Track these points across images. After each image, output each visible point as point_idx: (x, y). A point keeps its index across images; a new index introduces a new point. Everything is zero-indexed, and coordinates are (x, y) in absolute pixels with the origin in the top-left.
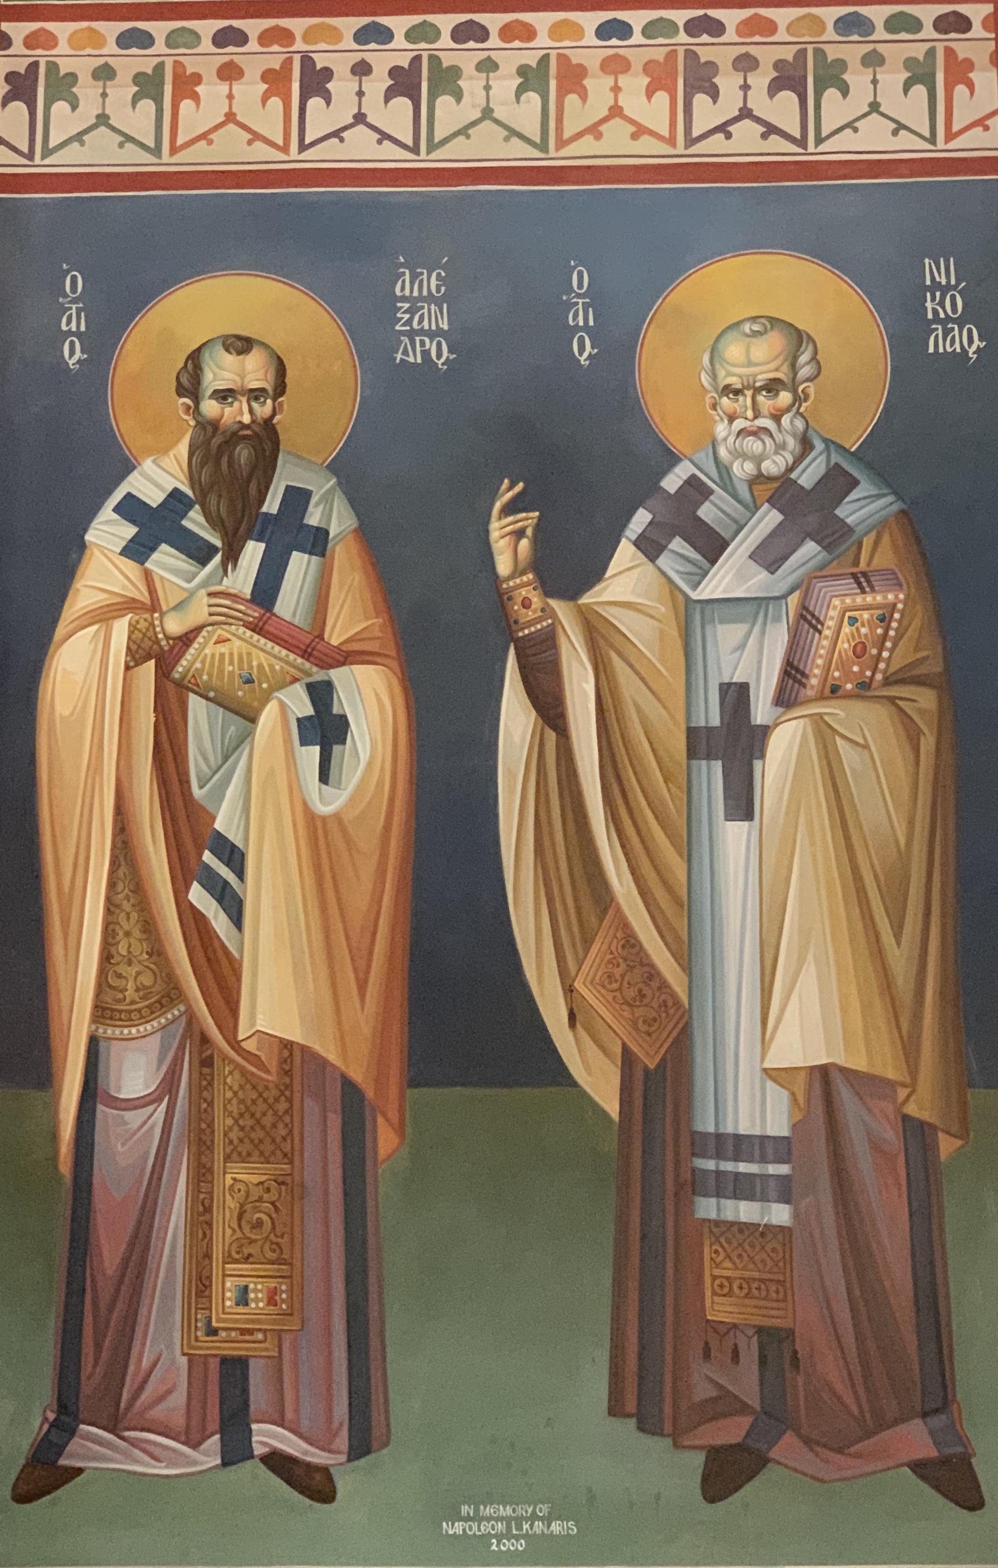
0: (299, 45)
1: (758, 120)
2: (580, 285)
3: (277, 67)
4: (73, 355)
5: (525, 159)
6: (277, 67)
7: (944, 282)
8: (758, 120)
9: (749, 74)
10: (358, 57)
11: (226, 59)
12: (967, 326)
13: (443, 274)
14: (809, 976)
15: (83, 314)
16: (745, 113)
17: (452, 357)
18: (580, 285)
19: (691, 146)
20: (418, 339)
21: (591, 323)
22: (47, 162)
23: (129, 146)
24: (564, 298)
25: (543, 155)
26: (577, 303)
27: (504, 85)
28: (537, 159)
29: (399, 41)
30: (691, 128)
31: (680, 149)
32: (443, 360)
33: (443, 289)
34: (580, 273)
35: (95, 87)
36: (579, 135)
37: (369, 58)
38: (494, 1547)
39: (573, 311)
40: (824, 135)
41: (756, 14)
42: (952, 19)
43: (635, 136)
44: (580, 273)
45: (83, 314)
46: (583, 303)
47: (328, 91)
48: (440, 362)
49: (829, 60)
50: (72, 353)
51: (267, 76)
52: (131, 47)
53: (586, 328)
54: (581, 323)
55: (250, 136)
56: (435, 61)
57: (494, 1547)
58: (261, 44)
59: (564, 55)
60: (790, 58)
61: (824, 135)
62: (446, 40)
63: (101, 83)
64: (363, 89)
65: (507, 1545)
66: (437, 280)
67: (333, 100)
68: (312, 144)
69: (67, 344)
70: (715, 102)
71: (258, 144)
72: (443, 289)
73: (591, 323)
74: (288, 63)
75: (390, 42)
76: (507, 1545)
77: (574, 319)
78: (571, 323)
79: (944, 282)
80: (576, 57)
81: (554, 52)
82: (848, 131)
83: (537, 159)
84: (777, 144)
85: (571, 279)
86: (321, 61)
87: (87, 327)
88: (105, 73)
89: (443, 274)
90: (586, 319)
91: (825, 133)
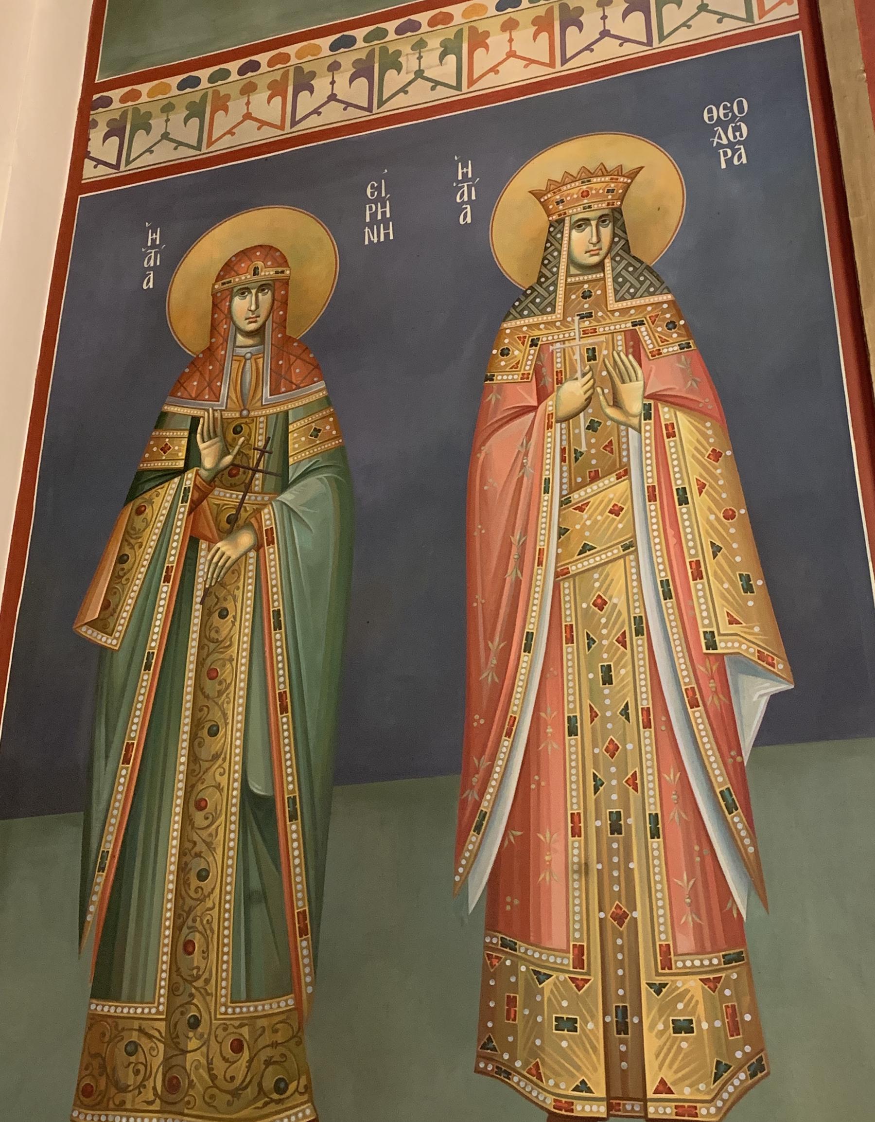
0: (294, 61)
1: (256, 120)
3: (543, 14)
4: (466, 217)
5: (775, 20)
6: (543, 14)
8: (256, 120)
9: (606, 7)
10: (330, 60)
11: (507, 17)
12: (743, 139)
13: (376, 185)
15: (159, 255)
16: (605, 33)
19: (472, 85)
20: (721, 151)
22: (471, 89)
23: (100, 166)
24: (143, 250)
25: (459, 93)
27: (431, 57)
28: (744, 27)
29: (360, 43)
30: (382, 94)
31: (204, 150)
35: (414, 54)
36: (773, 8)
37: (339, 59)
40: (568, 56)
41: (132, 89)
42: (440, 16)
43: (720, 21)
45: (159, 255)
47: (487, 44)
49: (142, 113)
51: (535, 21)
52: (128, 102)
55: (175, 145)
56: (384, 50)
58: (179, 89)
59: (472, 26)
60: (278, 78)
61: (568, 56)
62: (392, 36)
63: (165, 114)
64: (606, 14)
66: (371, 189)
67: (490, 49)
68: (134, 160)
70: (148, 134)
71: (533, 66)
74: (285, 75)
75: (139, 97)
80: (482, 27)
81: (467, 26)
82: (492, 74)
83: (744, 27)
84: (353, 113)
86: (307, 68)
88: (168, 108)
91: (476, 75)
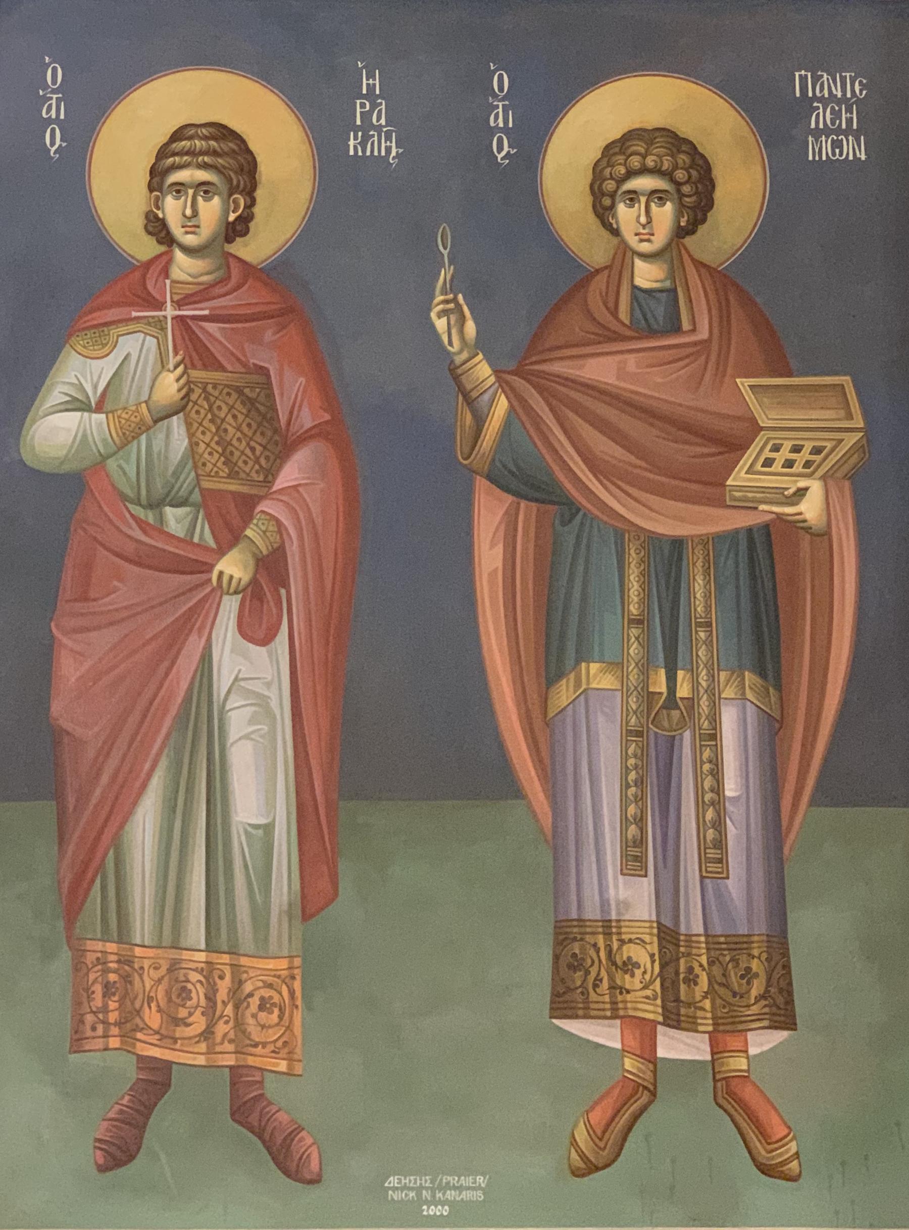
2: (54, 81)
4: (53, 140)
7: (839, 95)
13: (865, 81)
14: (685, 685)
17: (401, 151)
18: (54, 81)
21: (62, 117)
26: (497, 107)
32: (503, 153)
33: (864, 92)
34: (54, 70)
38: (425, 1213)
39: (46, 106)
44: (54, 70)
46: (57, 98)
48: (500, 157)
50: (500, 149)
53: (506, 130)
54: (501, 125)
57: (425, 1213)
65: (433, 1211)
69: (49, 131)
72: (864, 92)
73: (62, 117)
76: (433, 1211)
77: (48, 113)
78: (44, 115)
79: (839, 95)
85: (46, 75)
87: (362, 121)
89: (865, 81)
90: (506, 121)
